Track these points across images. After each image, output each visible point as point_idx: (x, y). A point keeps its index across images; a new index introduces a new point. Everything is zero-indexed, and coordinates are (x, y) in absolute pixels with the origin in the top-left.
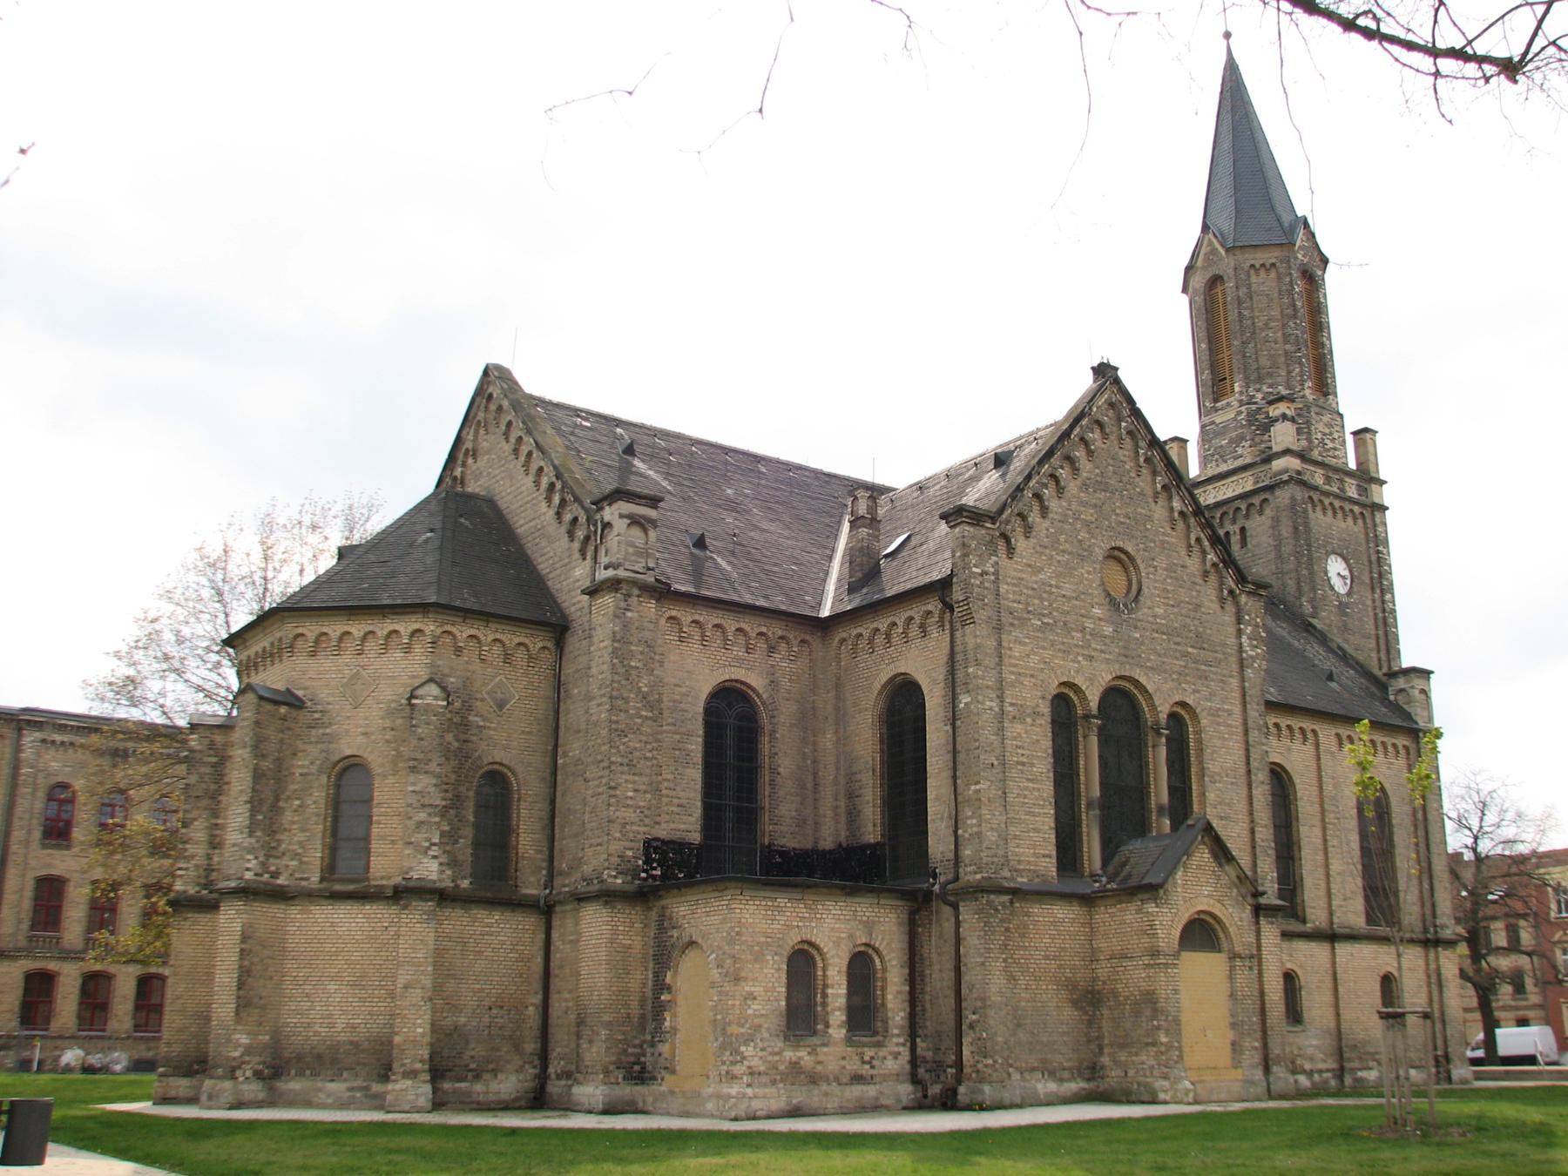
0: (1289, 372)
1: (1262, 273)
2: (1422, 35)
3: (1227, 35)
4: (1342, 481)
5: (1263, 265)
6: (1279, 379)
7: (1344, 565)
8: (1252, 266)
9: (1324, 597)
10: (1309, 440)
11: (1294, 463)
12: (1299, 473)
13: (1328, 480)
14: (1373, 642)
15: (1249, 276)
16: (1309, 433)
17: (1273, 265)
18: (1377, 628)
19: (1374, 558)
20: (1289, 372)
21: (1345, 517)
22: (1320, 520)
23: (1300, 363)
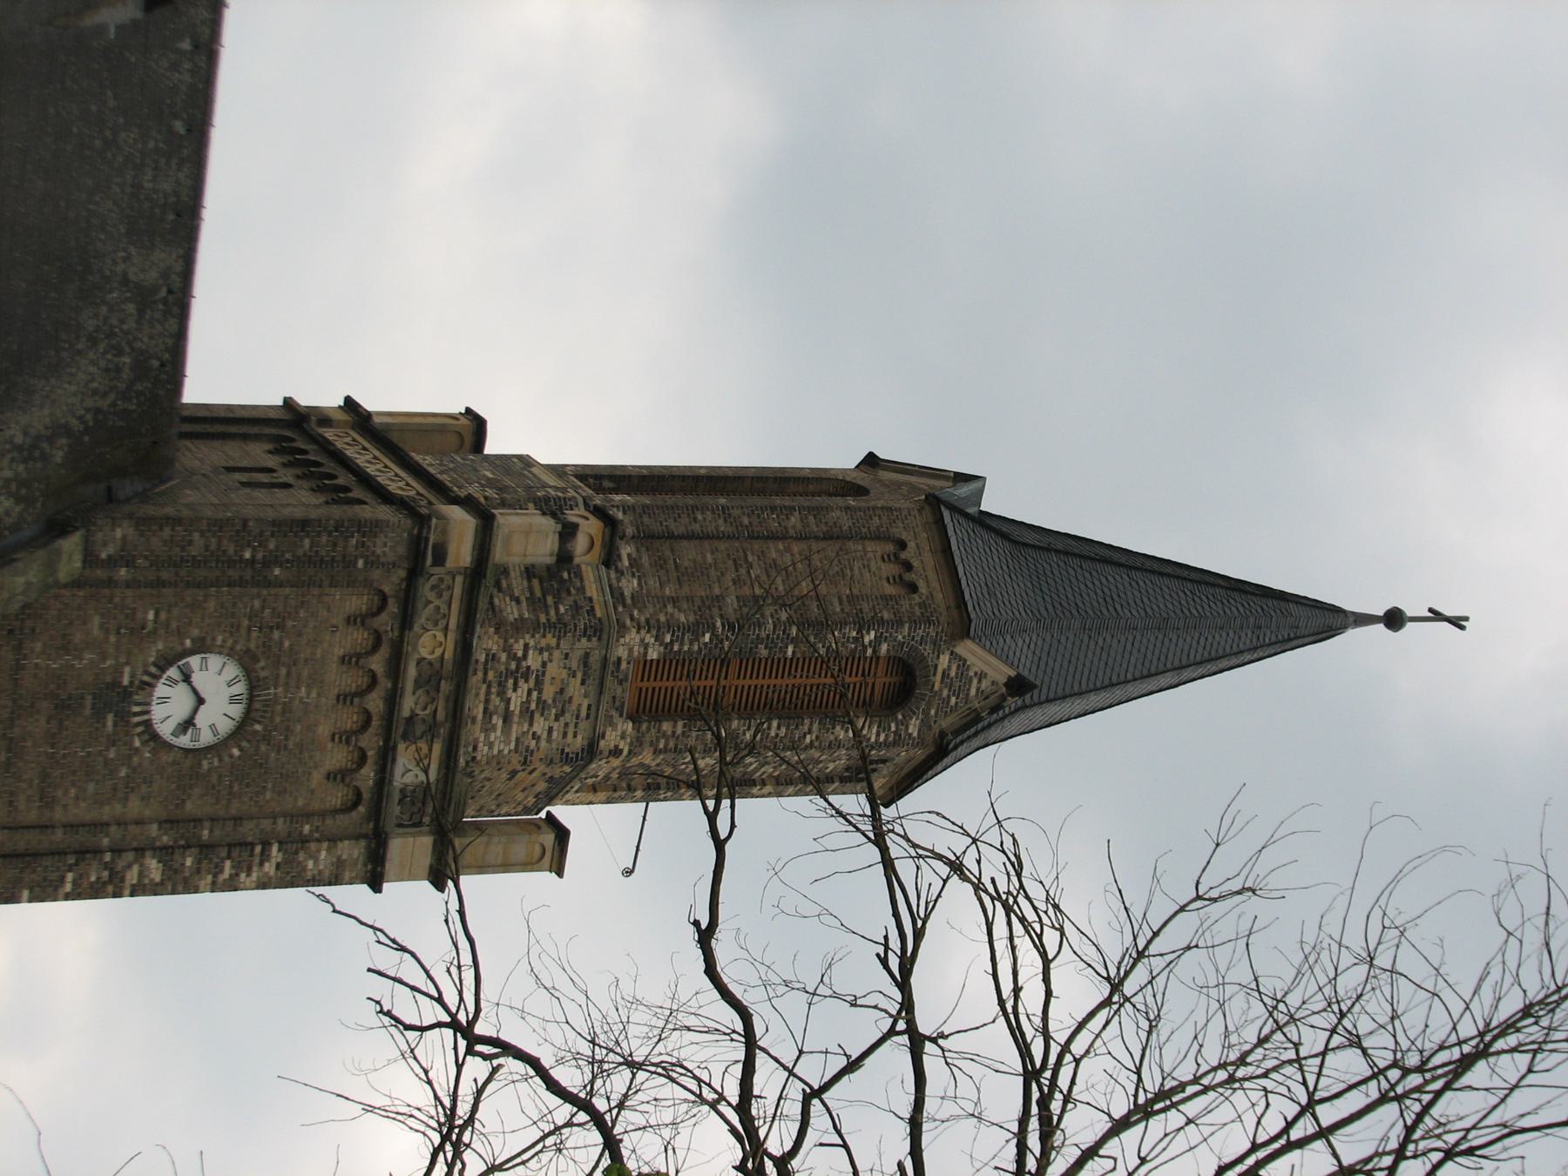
0: (674, 601)
1: (890, 569)
2: (1497, 1100)
3: (1394, 619)
4: (431, 730)
5: (908, 566)
6: (653, 583)
7: (225, 726)
8: (902, 545)
9: (140, 634)
10: (519, 626)
11: (462, 551)
12: (440, 557)
13: (430, 679)
14: (32, 816)
15: (877, 537)
16: (536, 627)
17: (913, 588)
18: (71, 827)
19: (249, 830)
20: (674, 601)
21: (343, 737)
22: (330, 629)
23: (695, 630)
